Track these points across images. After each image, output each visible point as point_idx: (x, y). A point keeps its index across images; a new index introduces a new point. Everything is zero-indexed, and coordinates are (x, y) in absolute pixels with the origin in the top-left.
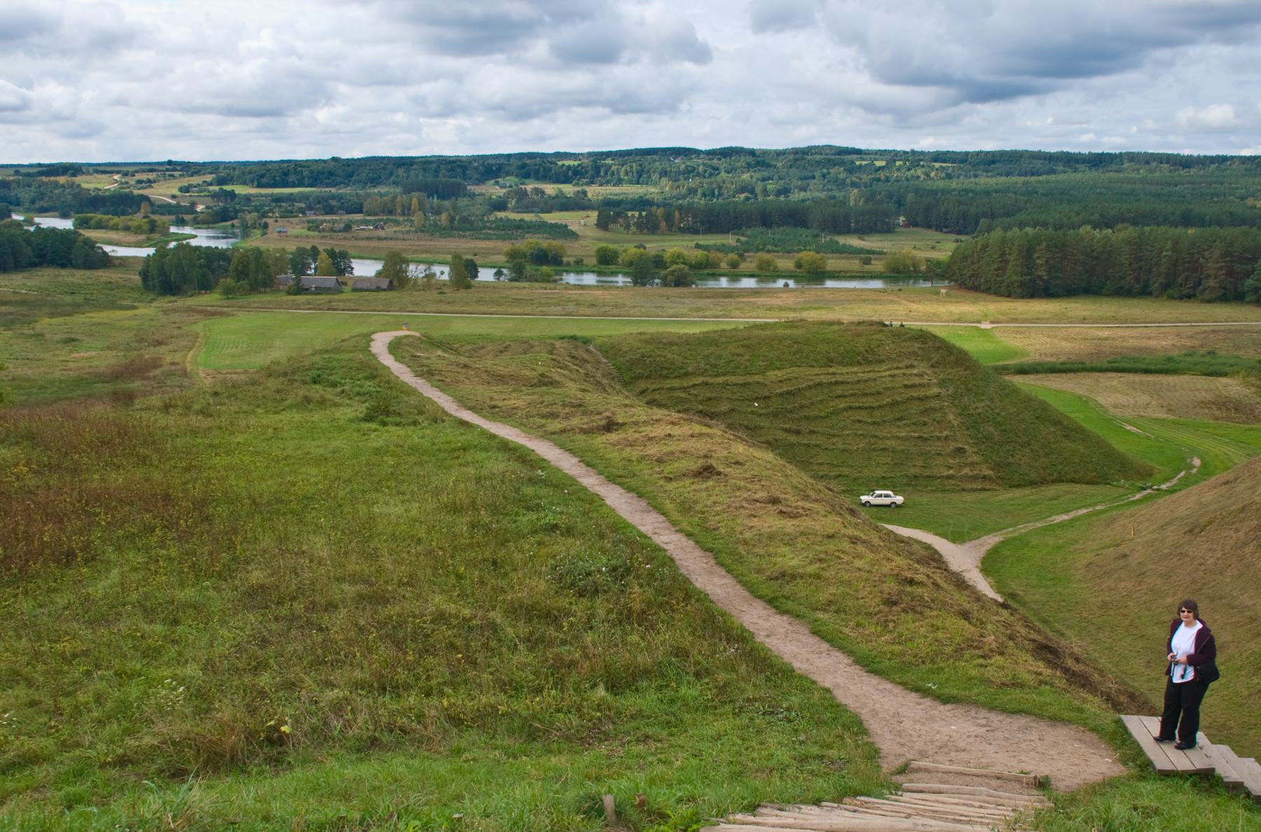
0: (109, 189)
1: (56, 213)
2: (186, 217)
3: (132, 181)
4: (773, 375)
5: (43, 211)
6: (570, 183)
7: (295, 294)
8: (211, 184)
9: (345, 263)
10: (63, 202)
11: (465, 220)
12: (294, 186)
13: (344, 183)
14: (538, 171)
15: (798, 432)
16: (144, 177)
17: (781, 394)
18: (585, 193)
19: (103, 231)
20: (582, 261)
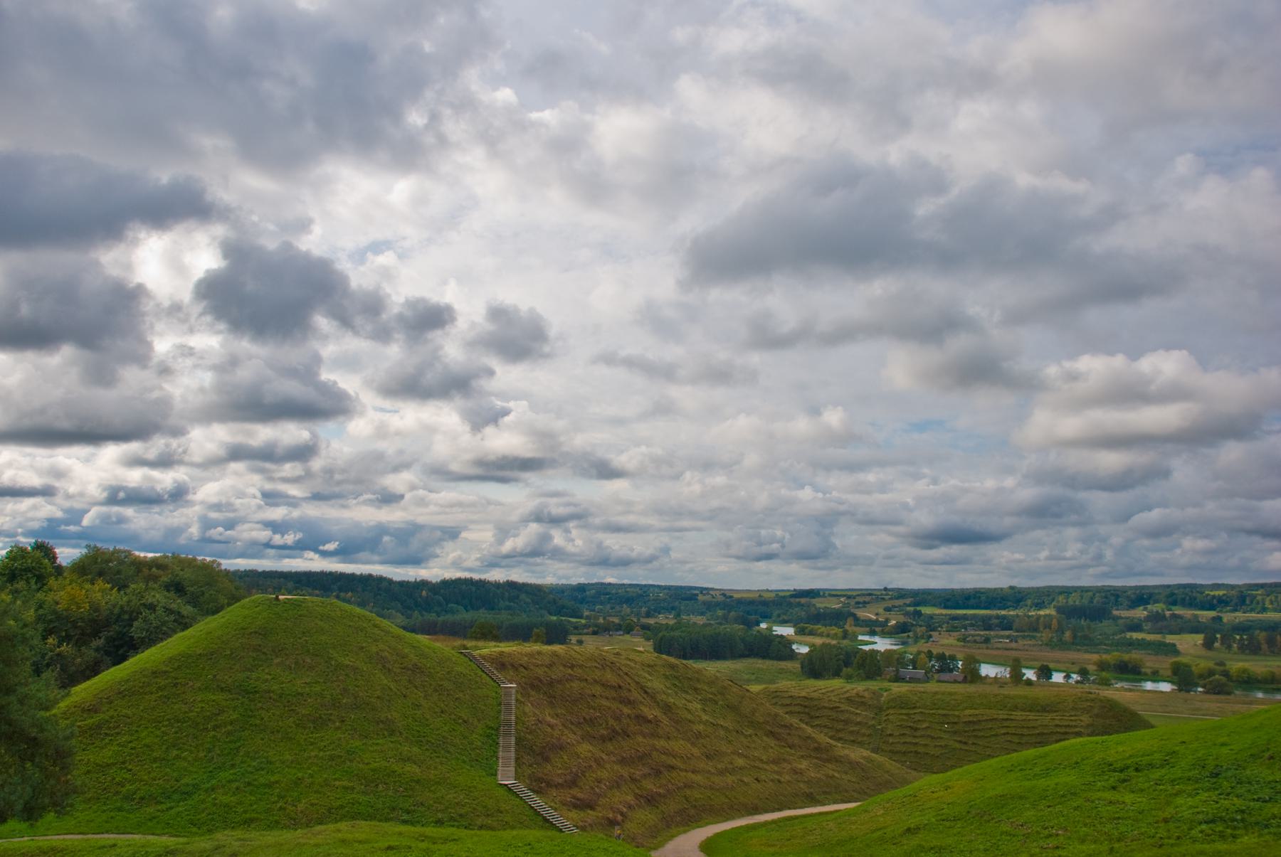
0: (834, 608)
1: (792, 624)
2: (877, 629)
3: (852, 602)
4: (967, 712)
5: (784, 623)
6: (1214, 610)
7: (894, 682)
8: (909, 606)
9: (954, 664)
10: (798, 616)
11: (1086, 637)
12: (973, 608)
13: (1013, 607)
14: (1184, 599)
15: (965, 743)
16: (860, 599)
17: (965, 722)
18: (1220, 618)
19: (812, 637)
20: (1157, 672)
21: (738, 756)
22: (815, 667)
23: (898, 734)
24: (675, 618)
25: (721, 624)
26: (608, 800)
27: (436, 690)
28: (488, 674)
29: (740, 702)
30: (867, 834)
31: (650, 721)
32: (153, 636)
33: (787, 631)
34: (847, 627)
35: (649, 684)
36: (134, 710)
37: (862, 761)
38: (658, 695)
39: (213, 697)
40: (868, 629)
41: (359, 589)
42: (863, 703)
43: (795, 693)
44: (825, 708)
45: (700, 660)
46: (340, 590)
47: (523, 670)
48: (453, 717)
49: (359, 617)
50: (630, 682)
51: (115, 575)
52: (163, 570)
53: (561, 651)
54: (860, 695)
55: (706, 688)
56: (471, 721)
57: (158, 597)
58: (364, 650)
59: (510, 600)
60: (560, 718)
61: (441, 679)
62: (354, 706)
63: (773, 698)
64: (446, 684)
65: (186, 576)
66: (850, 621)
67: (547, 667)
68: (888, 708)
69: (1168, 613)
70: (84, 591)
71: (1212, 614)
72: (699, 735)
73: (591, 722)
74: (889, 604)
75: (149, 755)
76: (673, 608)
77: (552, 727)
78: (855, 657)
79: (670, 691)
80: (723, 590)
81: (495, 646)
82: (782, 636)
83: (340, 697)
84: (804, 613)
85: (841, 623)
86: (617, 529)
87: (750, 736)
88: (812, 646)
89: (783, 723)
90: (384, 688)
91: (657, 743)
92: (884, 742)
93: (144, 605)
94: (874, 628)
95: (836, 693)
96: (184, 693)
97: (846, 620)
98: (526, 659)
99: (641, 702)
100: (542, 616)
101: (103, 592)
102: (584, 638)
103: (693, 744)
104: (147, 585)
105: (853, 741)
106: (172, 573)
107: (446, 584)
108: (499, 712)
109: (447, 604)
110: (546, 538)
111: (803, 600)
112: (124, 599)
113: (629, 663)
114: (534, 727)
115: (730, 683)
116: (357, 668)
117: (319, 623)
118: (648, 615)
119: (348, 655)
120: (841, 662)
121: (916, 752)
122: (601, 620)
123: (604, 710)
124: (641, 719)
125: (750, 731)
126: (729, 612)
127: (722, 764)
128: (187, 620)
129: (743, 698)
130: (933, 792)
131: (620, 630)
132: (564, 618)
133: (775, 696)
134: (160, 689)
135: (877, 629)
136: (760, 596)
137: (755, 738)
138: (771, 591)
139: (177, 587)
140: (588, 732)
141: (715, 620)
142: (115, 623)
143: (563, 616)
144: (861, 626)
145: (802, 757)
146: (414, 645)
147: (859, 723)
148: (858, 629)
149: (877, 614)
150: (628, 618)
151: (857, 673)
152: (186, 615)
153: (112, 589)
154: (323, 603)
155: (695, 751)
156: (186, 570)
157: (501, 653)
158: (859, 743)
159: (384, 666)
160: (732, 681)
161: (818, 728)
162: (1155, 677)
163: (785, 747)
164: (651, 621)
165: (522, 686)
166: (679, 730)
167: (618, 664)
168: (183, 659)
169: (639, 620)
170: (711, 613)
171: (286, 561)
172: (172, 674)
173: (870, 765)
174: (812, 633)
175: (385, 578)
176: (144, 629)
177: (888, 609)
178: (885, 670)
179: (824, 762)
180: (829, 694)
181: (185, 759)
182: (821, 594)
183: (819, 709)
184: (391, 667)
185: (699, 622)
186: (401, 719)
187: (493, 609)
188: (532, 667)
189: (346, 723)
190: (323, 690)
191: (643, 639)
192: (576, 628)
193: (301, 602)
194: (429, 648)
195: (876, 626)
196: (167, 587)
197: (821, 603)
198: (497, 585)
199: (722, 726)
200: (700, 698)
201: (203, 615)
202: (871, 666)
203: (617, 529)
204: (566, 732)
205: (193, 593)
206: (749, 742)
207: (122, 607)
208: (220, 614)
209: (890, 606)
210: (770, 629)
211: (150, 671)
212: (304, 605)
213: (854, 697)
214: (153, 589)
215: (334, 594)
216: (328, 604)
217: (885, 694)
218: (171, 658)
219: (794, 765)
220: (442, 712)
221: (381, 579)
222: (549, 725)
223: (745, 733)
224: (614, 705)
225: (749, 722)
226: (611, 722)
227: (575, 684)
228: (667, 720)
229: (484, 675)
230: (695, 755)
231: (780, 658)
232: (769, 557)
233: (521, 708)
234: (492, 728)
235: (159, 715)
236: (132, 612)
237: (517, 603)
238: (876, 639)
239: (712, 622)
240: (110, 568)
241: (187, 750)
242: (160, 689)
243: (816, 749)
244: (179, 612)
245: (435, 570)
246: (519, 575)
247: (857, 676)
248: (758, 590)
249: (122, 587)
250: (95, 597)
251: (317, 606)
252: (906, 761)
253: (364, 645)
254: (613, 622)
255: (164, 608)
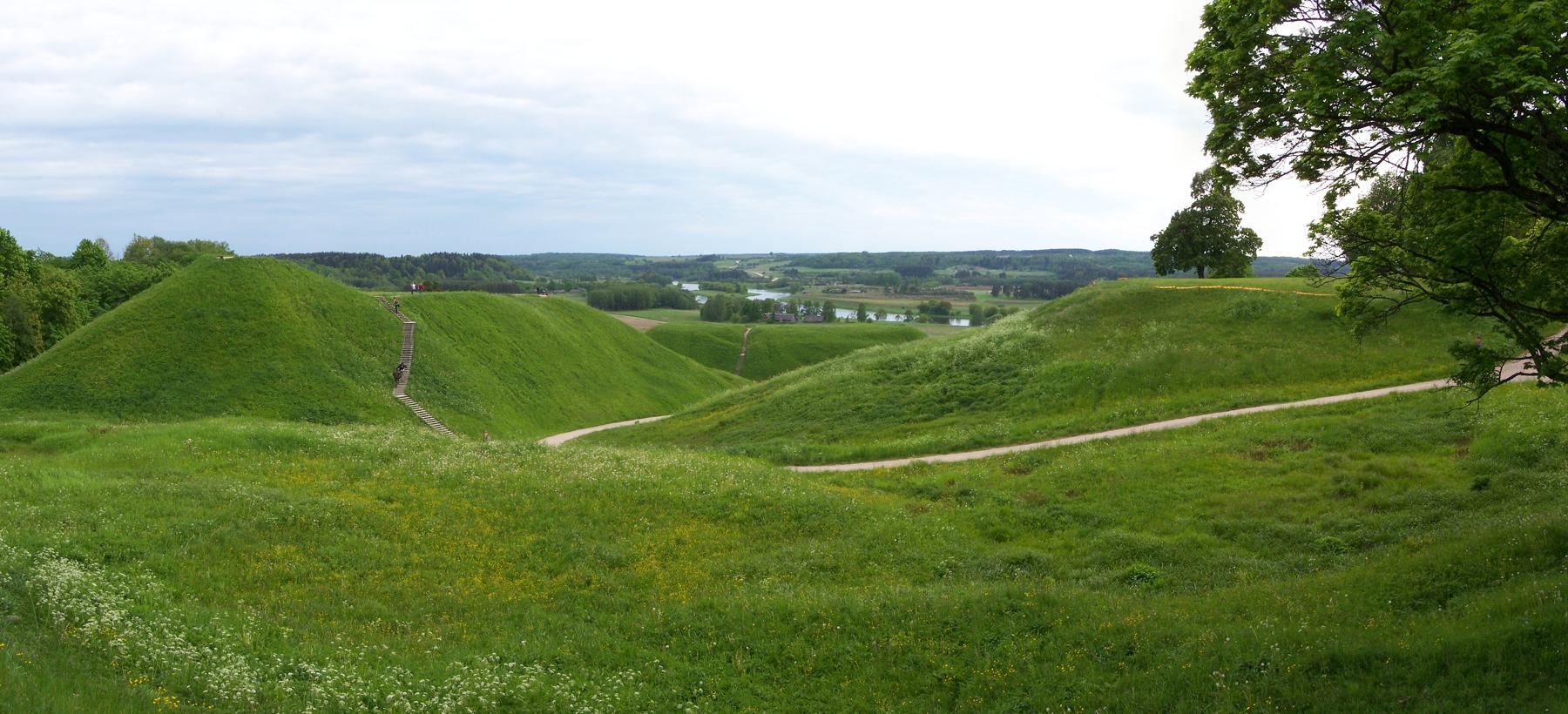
3: (745, 264)
5: (690, 281)
16: (752, 262)
22: (710, 313)
33: (692, 287)
69: (971, 271)
71: (1000, 272)
74: (772, 265)
82: (687, 291)
94: (761, 284)
149: (764, 273)
162: (958, 316)
175: (379, 255)
177: (772, 269)
202: (754, 312)
210: (680, 285)
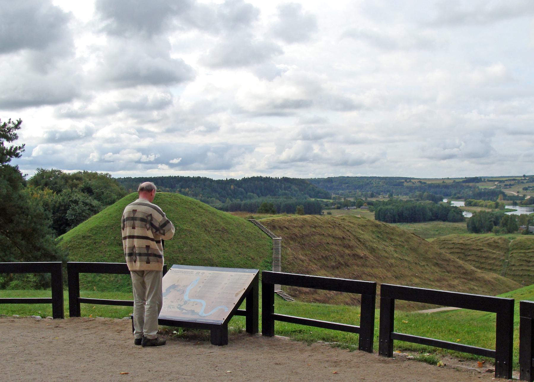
0: (491, 189)
3: (503, 185)
5: (458, 199)
10: (467, 194)
19: (476, 207)
21: (415, 277)
23: (518, 264)
24: (389, 197)
25: (418, 200)
26: (334, 301)
27: (235, 242)
28: (265, 233)
29: (418, 246)
30: (481, 317)
31: (362, 258)
32: (78, 218)
33: (459, 204)
34: (498, 201)
35: (362, 236)
36: (75, 257)
37: (492, 280)
38: (367, 243)
39: (115, 249)
40: (512, 202)
41: (193, 186)
42: (498, 247)
43: (456, 241)
44: (474, 249)
45: (405, 223)
46: (182, 187)
47: (287, 230)
48: (246, 256)
49: (190, 202)
50: (350, 235)
51: (54, 185)
52: (79, 181)
53: (309, 218)
54: (496, 241)
55: (398, 238)
56: (256, 258)
57: (79, 196)
58: (194, 221)
59: (285, 189)
60: (308, 256)
61: (238, 236)
62: (191, 252)
63: (442, 244)
64: (241, 238)
65: (92, 184)
66: (500, 196)
67: (300, 227)
68: (513, 249)
70: (39, 195)
72: (391, 265)
73: (326, 258)
74: (526, 186)
75: (85, 280)
76: (388, 191)
77: (303, 261)
78: (501, 219)
79: (375, 240)
80: (420, 179)
81: (270, 216)
82: (456, 207)
83: (182, 247)
84: (471, 192)
85: (495, 198)
86: (354, 142)
87: (424, 266)
88: (474, 213)
89: (444, 258)
90: (206, 242)
91: (365, 270)
92: (509, 270)
93: (71, 201)
94: (515, 201)
95: (481, 240)
96: (100, 247)
97: (498, 196)
98: (287, 223)
99: (356, 247)
100: (306, 198)
101: (49, 195)
102: (332, 211)
103: (388, 271)
104: (72, 190)
105: (491, 269)
106: (85, 182)
107: (245, 180)
108: (272, 253)
109: (247, 193)
110: (309, 149)
111: (471, 184)
112: (61, 198)
113: (350, 224)
114: (292, 261)
115: (413, 235)
116: (191, 231)
117: (169, 207)
118: (372, 196)
119: (185, 224)
120: (492, 223)
121: (529, 275)
122: (343, 200)
123: (334, 251)
124: (356, 256)
125: (424, 263)
126: (423, 193)
127: (405, 282)
128: (96, 209)
129: (420, 243)
130: (522, 294)
131: (354, 205)
132: (319, 199)
133: (443, 243)
134: (87, 245)
135: (518, 202)
136: (443, 182)
137: (427, 267)
138: (451, 179)
139: (88, 190)
140: (324, 264)
141: (414, 198)
142: (57, 212)
143: (318, 198)
144: (508, 200)
145: (455, 278)
146: (222, 217)
147: (494, 258)
148: (504, 202)
149: (518, 192)
150: (359, 198)
151: (502, 229)
152: (95, 206)
153: (53, 193)
154: (170, 195)
155: (389, 274)
156: (92, 180)
157: (273, 221)
158: (494, 270)
159: (206, 229)
160: (414, 234)
161: (469, 262)
163: (445, 272)
164: (374, 200)
165: (285, 239)
166: (379, 263)
167: (343, 225)
168: (97, 229)
169: (366, 199)
170: (412, 194)
171: (149, 171)
172: (93, 237)
173: (497, 282)
174: (476, 205)
176: (73, 215)
177: (525, 189)
178: (520, 227)
179: (468, 281)
180: (477, 241)
181: (104, 281)
182: (483, 180)
183: (470, 250)
184: (210, 230)
185: (403, 200)
186: (217, 258)
187: (275, 195)
188: (291, 228)
189: (186, 261)
190: (173, 243)
191: (369, 211)
192: (327, 205)
193: (159, 195)
194: (231, 218)
195: (517, 200)
196: (83, 190)
197: (483, 186)
198: (277, 180)
199: (406, 260)
200: (393, 244)
201: (104, 206)
203: (354, 142)
204: (311, 264)
205: (97, 193)
206: (423, 269)
207: (60, 203)
208: (115, 204)
209: (527, 187)
210: (449, 203)
211: (82, 236)
212: (159, 197)
213: (492, 243)
214: (76, 192)
215: (178, 189)
216: (173, 196)
217: (512, 241)
218: (91, 229)
219: (450, 282)
220: (239, 254)
221: (205, 179)
222: (301, 260)
223: (420, 264)
224: (340, 249)
225: (423, 257)
226: (338, 258)
227: (317, 237)
228: (372, 256)
229: (263, 233)
230: (388, 276)
231: (454, 221)
232: (451, 157)
233: (285, 251)
234: (268, 262)
235: (88, 259)
236: (66, 205)
237: (290, 191)
238: (517, 208)
239: (412, 199)
240: (51, 181)
241: (104, 277)
242: (87, 245)
243: (464, 273)
244: (91, 204)
245: (240, 172)
246: (291, 174)
247: (502, 231)
248: (442, 179)
249: (59, 191)
250: (45, 198)
251: (167, 197)
252: (522, 281)
253: (194, 218)
254: (350, 201)
255: (83, 202)
